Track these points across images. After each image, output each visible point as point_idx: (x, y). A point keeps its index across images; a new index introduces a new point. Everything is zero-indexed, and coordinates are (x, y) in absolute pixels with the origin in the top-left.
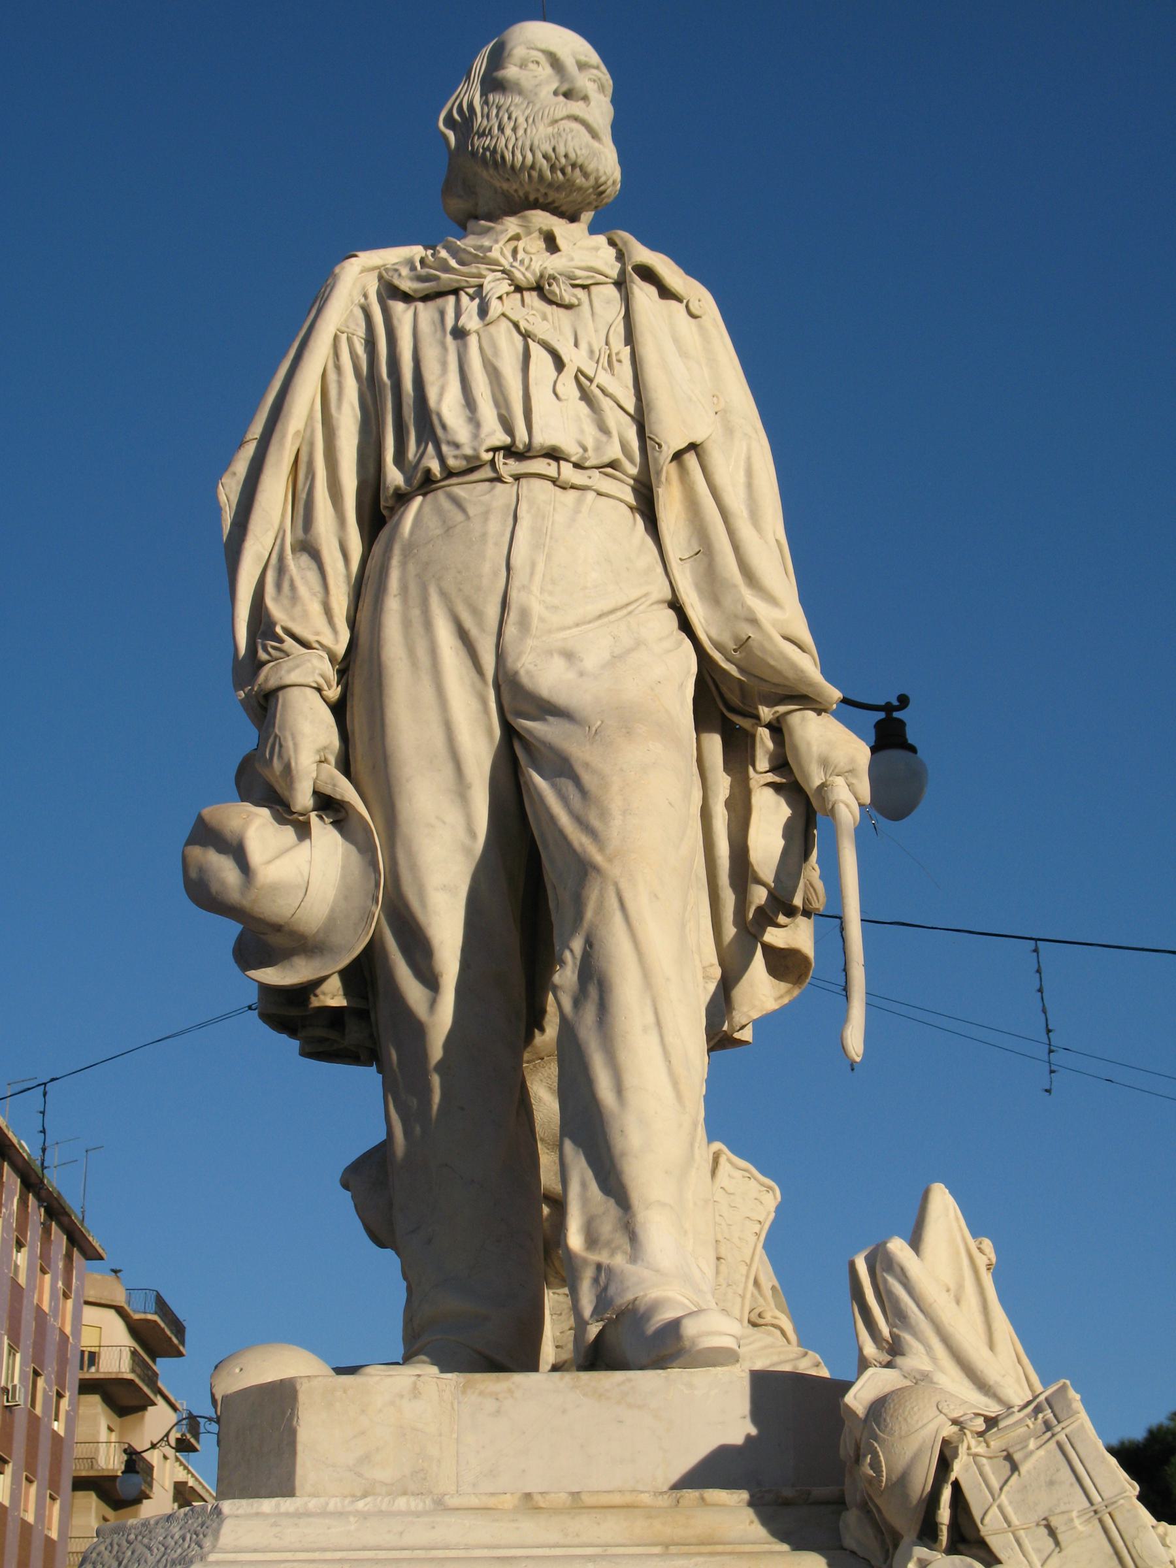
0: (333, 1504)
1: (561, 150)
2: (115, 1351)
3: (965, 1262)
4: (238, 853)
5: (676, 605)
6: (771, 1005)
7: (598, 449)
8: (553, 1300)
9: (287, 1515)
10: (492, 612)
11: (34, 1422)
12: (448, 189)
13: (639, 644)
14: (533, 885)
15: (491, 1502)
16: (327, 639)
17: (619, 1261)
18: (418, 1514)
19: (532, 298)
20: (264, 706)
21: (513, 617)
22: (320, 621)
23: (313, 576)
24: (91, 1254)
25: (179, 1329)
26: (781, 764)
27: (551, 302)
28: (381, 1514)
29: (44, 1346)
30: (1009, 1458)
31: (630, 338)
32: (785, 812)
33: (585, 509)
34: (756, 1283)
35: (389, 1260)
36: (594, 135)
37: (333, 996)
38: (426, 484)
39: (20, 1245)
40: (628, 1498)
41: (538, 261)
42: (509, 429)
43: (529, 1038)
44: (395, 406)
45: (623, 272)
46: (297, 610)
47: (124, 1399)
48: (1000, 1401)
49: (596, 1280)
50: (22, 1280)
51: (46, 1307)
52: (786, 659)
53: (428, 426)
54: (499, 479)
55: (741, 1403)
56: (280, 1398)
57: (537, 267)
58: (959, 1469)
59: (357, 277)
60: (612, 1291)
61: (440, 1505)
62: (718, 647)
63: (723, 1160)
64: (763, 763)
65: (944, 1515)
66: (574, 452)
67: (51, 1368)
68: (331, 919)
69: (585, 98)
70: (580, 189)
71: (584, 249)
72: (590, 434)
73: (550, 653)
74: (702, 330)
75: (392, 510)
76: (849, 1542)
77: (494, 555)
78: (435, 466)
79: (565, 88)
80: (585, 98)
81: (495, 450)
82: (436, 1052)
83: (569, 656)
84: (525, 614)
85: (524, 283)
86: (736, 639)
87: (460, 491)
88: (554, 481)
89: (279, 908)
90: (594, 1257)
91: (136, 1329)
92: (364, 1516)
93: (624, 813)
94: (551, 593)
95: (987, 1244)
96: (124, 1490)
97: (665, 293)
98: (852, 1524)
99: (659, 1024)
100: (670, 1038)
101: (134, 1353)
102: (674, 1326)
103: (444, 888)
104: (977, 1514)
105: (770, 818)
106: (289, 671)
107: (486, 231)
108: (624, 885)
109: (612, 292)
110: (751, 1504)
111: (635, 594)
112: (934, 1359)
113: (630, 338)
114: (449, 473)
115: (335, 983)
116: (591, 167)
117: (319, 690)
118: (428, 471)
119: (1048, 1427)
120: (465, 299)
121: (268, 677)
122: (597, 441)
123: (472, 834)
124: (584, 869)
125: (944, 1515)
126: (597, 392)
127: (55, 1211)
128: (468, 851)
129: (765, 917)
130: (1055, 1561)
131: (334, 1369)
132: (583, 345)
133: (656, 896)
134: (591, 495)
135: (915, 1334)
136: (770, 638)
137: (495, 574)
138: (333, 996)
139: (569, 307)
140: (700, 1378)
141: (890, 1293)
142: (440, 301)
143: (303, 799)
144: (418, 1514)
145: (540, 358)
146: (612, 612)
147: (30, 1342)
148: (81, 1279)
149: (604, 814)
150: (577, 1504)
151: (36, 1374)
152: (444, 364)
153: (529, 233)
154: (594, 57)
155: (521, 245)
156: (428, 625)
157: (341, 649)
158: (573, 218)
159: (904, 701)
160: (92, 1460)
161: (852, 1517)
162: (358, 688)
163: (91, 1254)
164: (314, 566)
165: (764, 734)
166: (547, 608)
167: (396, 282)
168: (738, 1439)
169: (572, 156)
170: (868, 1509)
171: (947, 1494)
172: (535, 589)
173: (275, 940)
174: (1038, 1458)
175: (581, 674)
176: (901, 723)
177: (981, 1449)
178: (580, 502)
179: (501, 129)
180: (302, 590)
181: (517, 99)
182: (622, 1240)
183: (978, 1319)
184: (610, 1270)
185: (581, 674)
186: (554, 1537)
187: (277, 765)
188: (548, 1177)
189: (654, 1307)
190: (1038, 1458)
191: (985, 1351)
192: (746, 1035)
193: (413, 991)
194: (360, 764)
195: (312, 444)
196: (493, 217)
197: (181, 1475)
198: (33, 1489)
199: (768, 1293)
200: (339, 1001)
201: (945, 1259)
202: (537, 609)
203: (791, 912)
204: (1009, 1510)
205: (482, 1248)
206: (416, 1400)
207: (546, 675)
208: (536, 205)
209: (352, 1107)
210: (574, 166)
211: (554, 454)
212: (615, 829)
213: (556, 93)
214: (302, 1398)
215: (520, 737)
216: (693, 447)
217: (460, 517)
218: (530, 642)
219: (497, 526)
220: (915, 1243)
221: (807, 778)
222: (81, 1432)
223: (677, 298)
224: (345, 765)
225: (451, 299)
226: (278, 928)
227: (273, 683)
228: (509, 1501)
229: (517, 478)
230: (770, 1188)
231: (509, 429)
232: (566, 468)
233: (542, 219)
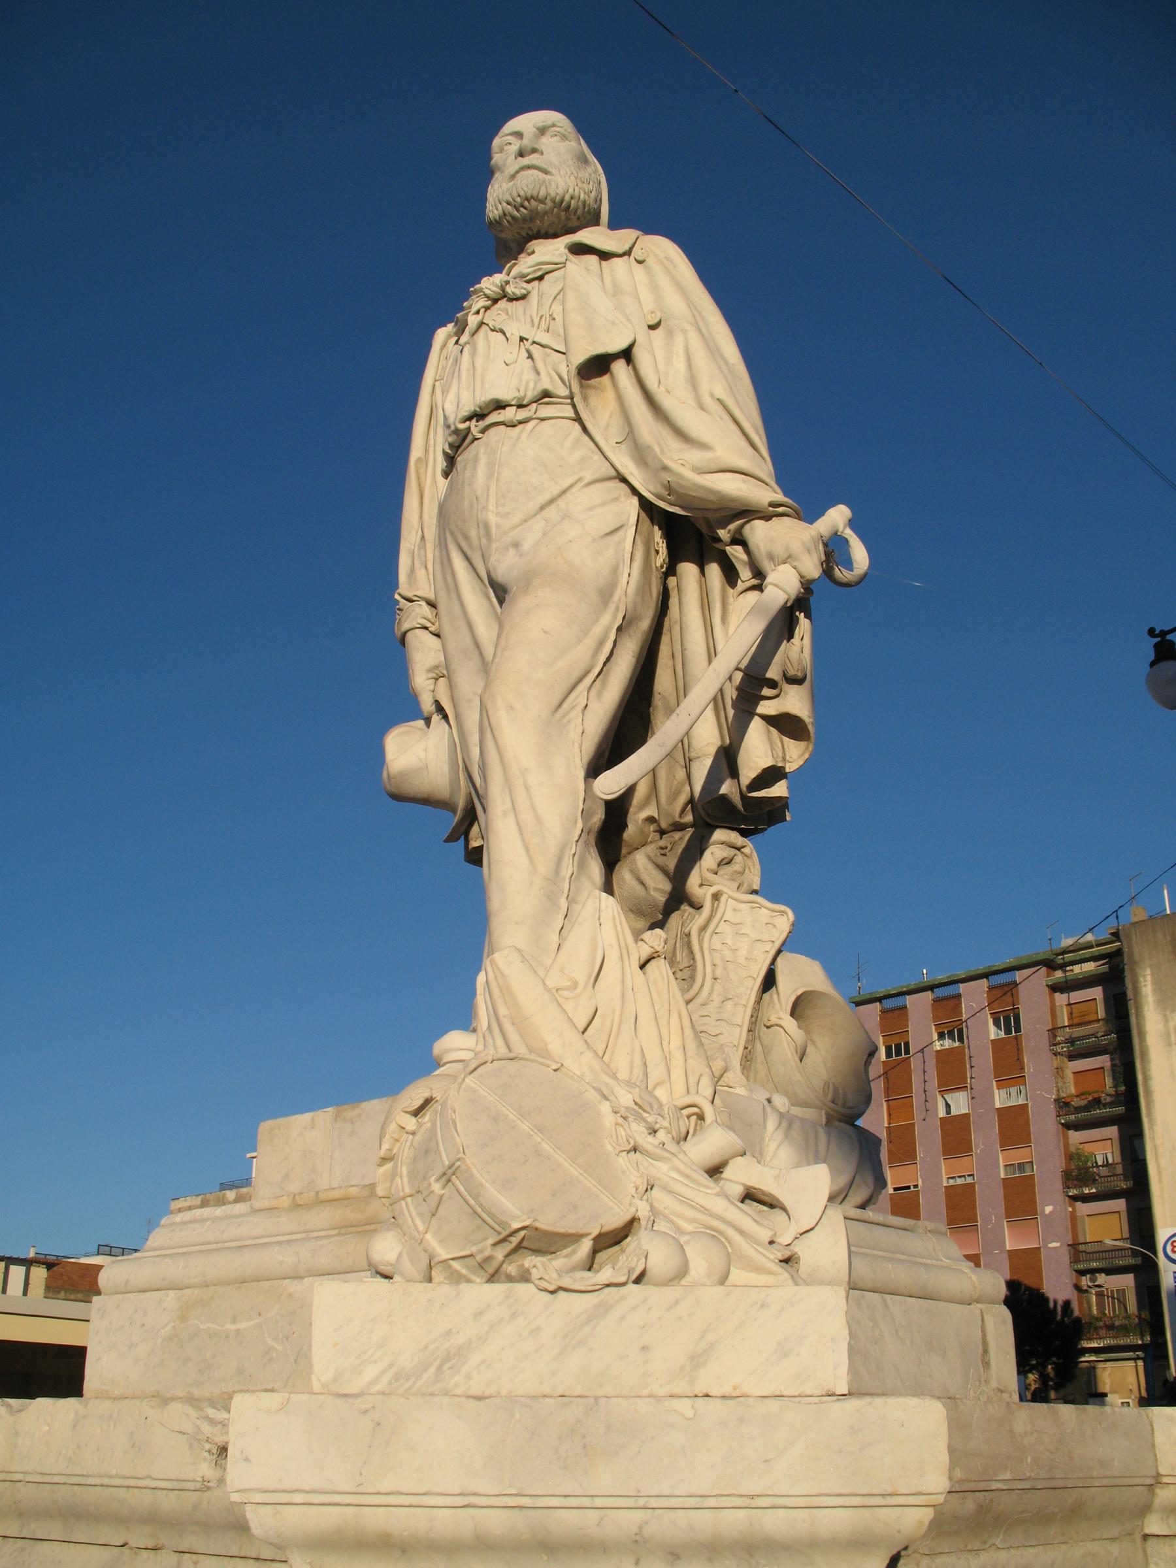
70: (545, 213)
73: (506, 549)
94: (504, 505)
99: (514, 807)
133: (512, 708)
143: (427, 706)
166: (502, 517)
169: (522, 193)
202: (493, 519)
210: (527, 199)
218: (494, 546)
230: (783, 913)
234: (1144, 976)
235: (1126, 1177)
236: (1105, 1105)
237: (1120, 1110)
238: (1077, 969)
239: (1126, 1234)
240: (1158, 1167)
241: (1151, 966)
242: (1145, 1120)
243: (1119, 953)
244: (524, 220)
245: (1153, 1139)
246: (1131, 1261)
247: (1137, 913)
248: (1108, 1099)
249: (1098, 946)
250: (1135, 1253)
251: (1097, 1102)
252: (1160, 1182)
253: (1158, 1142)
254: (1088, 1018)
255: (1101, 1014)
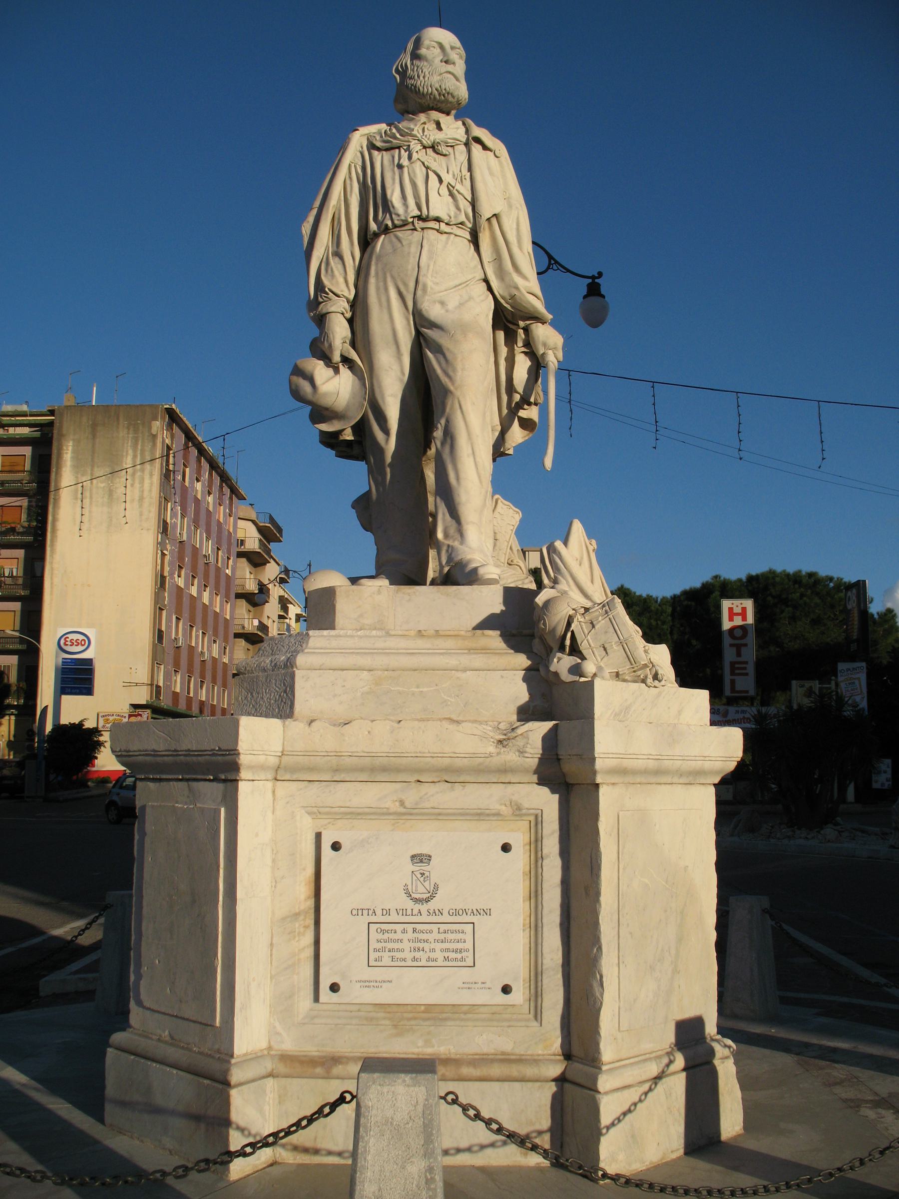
0: (349, 633)
1: (443, 87)
2: (252, 540)
3: (584, 548)
4: (311, 380)
5: (486, 281)
6: (520, 441)
7: (456, 217)
8: (432, 553)
9: (332, 636)
10: (412, 285)
11: (218, 569)
12: (396, 100)
13: (470, 298)
14: (427, 397)
15: (406, 633)
16: (346, 294)
17: (456, 544)
18: (380, 637)
19: (430, 151)
20: (321, 320)
21: (420, 287)
22: (343, 285)
23: (340, 266)
24: (241, 498)
25: (280, 530)
26: (528, 344)
27: (438, 154)
28: (366, 636)
29: (223, 538)
30: (592, 623)
31: (470, 169)
32: (529, 363)
33: (450, 243)
34: (511, 548)
35: (370, 536)
36: (457, 80)
37: (348, 436)
38: (386, 230)
39: (209, 493)
40: (456, 633)
41: (434, 135)
42: (420, 209)
43: (425, 452)
44: (373, 196)
45: (468, 139)
46: (334, 281)
47: (256, 560)
48: (592, 601)
49: (447, 551)
50: (211, 509)
51: (221, 521)
52: (530, 303)
53: (387, 206)
54: (415, 229)
55: (499, 598)
56: (329, 594)
57: (432, 138)
58: (573, 627)
59: (358, 139)
60: (453, 555)
61: (388, 634)
62: (503, 298)
63: (499, 502)
64: (520, 344)
65: (568, 642)
66: (445, 217)
67: (224, 547)
68: (348, 405)
69: (454, 63)
71: (453, 128)
72: (453, 209)
73: (435, 302)
74: (501, 163)
75: (373, 240)
76: (535, 650)
77: (413, 261)
78: (390, 223)
79: (445, 59)
80: (454, 63)
81: (414, 217)
82: (389, 459)
83: (442, 303)
84: (425, 286)
85: (427, 145)
86: (510, 295)
87: (399, 234)
88: (438, 231)
89: (327, 402)
90: (447, 542)
91: (260, 530)
92: (361, 637)
93: (463, 369)
95: (594, 542)
96: (257, 599)
97: (485, 148)
98: (536, 645)
99: (473, 453)
100: (478, 459)
101: (260, 540)
102: (475, 570)
103: (392, 395)
104: (579, 643)
105: (522, 365)
106: (331, 306)
107: (412, 120)
108: (461, 399)
109: (463, 148)
110: (501, 636)
111: (470, 277)
112: (569, 586)
113: (470, 169)
114: (395, 226)
115: (349, 431)
116: (455, 94)
117: (343, 314)
118: (387, 225)
119: (606, 612)
120: (403, 151)
121: (322, 308)
122: (455, 213)
123: (403, 374)
124: (446, 392)
125: (568, 642)
126: (456, 192)
127: (225, 478)
128: (401, 381)
129: (519, 406)
130: (605, 659)
131: (350, 579)
132: (451, 172)
134: (452, 236)
135: (563, 577)
136: (523, 295)
137: (413, 269)
138: (348, 436)
139: (445, 155)
140: (485, 589)
141: (555, 561)
142: (392, 151)
143: (337, 358)
144: (380, 637)
145: (433, 178)
146: (460, 285)
147: (215, 535)
148: (237, 508)
149: (454, 370)
150: (437, 634)
151: (218, 549)
152: (394, 179)
153: (430, 121)
154: (458, 43)
155: (426, 126)
156: (386, 289)
157: (351, 297)
158: (448, 114)
159: (600, 274)
160: (243, 586)
161: (536, 641)
162: (358, 313)
163: (241, 498)
164: (340, 262)
165: (521, 332)
167: (374, 142)
168: (498, 612)
170: (543, 640)
171: (569, 635)
172: (429, 276)
173: (326, 413)
174: (602, 623)
175: (447, 311)
176: (599, 285)
177: (582, 620)
178: (448, 239)
179: (419, 77)
180: (336, 273)
181: (425, 64)
182: (458, 536)
183: (588, 570)
184: (452, 547)
185: (447, 311)
186: (429, 645)
187: (326, 344)
188: (431, 507)
189: (469, 562)
190: (602, 623)
191: (589, 583)
192: (511, 452)
193: (379, 435)
194: (359, 344)
195: (340, 211)
196: (414, 113)
197: (282, 593)
198: (218, 598)
199: (516, 552)
200: (351, 438)
201: (578, 550)
202: (430, 284)
203: (529, 404)
204: (591, 641)
205: (405, 536)
206: (379, 589)
207: (434, 312)
208: (432, 109)
209: (355, 477)
211: (438, 220)
212: (459, 376)
213: (441, 61)
214: (337, 593)
215: (423, 336)
216: (495, 215)
217: (399, 245)
219: (414, 250)
220: (566, 543)
221: (538, 351)
222: (238, 574)
223: (490, 150)
224: (353, 344)
225: (397, 151)
226: (327, 409)
227: (324, 311)
228: (413, 633)
229: (423, 229)
231: (420, 209)
232: (443, 225)
233: (435, 115)
234: (67, 446)
235: (24, 586)
236: (19, 534)
237: (30, 538)
238: (11, 430)
239: (17, 627)
240: (52, 583)
241: (73, 440)
242: (48, 549)
243: (51, 424)
244: (438, 101)
245: (52, 563)
246: (19, 647)
247: (69, 400)
248: (21, 530)
249: (31, 415)
250: (22, 641)
251: (13, 530)
252: (52, 594)
253: (55, 566)
254: (17, 468)
255: (28, 467)
